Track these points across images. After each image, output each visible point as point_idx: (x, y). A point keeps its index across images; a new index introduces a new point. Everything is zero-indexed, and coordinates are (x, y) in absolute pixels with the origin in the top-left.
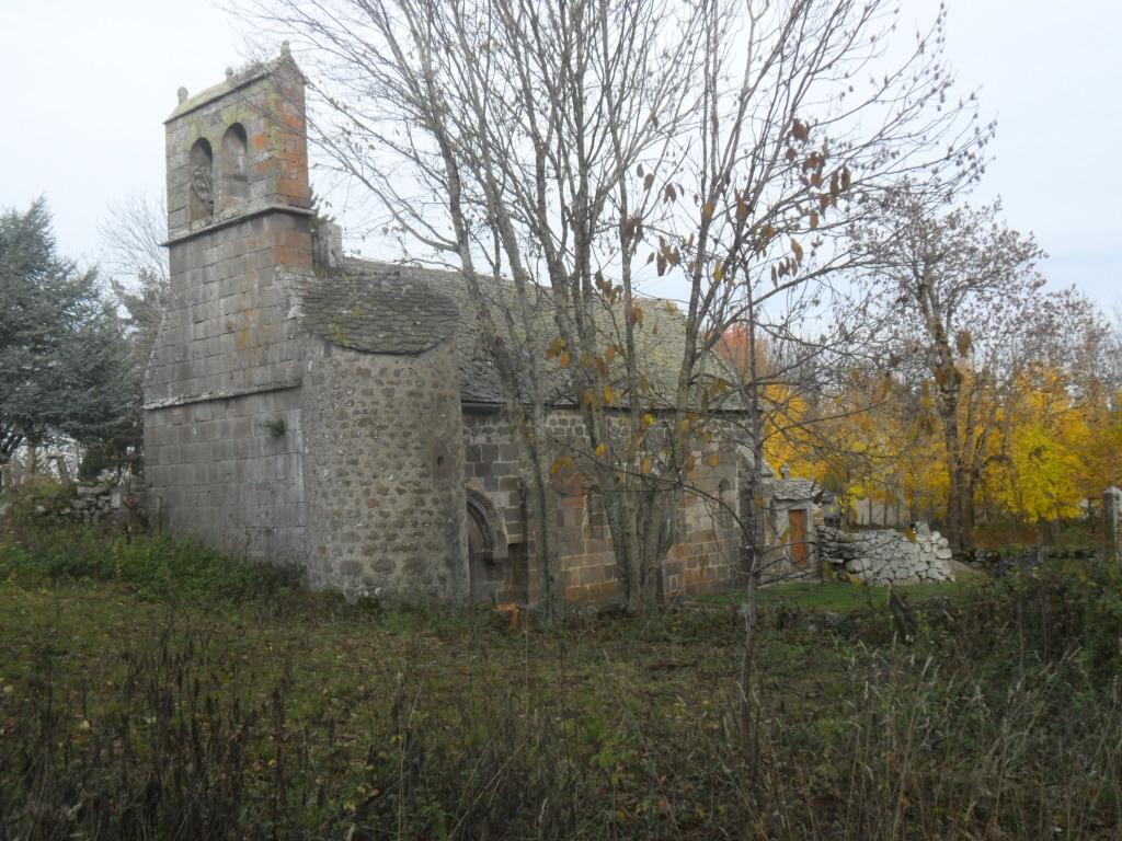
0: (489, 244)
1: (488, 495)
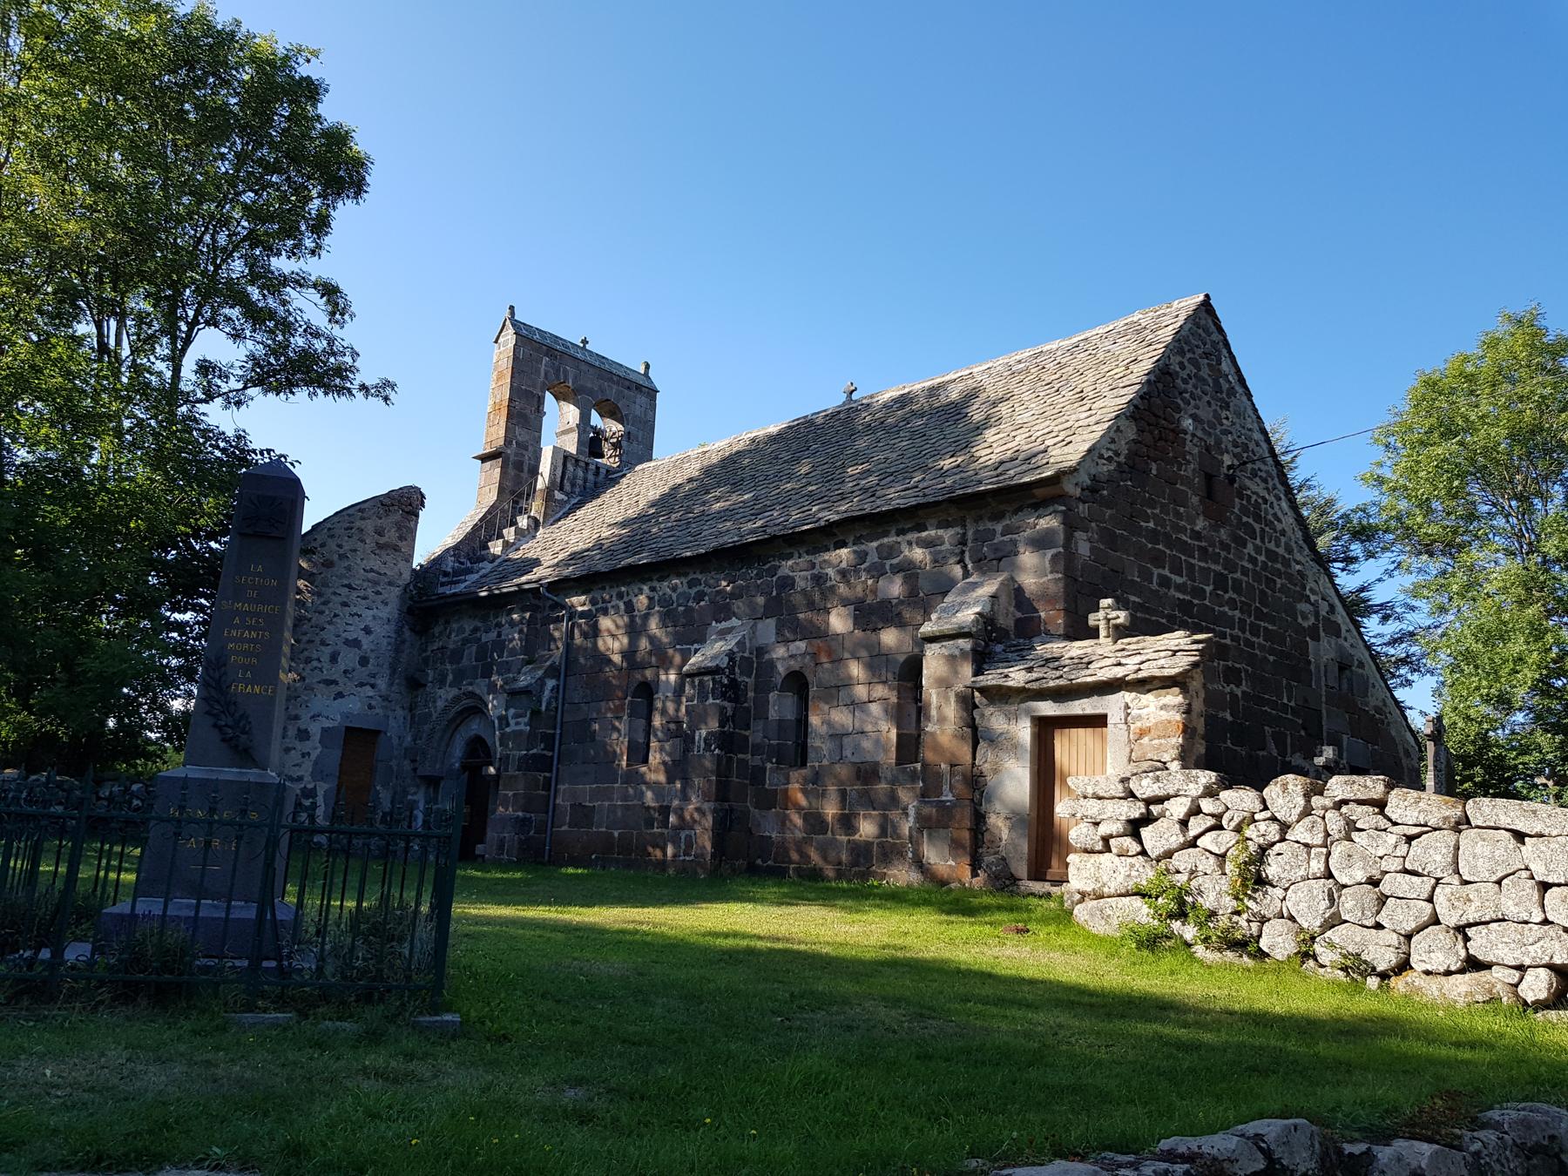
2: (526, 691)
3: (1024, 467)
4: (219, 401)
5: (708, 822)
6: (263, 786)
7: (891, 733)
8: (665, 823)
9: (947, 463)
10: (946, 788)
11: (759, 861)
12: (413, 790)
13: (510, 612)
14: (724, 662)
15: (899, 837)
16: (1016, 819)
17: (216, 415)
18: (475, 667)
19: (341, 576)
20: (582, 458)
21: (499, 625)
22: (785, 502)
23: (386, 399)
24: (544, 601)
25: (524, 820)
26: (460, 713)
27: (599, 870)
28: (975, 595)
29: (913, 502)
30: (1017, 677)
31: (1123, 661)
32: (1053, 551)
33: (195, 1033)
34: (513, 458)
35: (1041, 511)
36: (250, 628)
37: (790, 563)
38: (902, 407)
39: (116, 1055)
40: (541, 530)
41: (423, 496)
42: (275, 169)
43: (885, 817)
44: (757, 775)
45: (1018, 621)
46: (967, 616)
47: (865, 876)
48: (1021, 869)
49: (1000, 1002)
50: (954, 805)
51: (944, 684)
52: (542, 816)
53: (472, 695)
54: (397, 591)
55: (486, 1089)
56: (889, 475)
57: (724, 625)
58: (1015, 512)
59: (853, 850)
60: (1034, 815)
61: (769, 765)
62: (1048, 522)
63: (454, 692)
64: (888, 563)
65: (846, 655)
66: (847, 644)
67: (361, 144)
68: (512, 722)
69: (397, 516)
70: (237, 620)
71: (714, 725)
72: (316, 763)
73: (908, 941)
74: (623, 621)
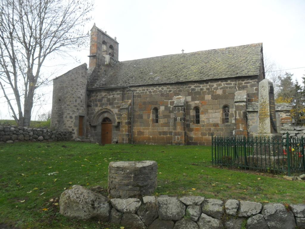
0: (33, 26)
1: (112, 110)
11: (190, 141)
31: (278, 107)
61: (191, 124)
72: (74, 123)
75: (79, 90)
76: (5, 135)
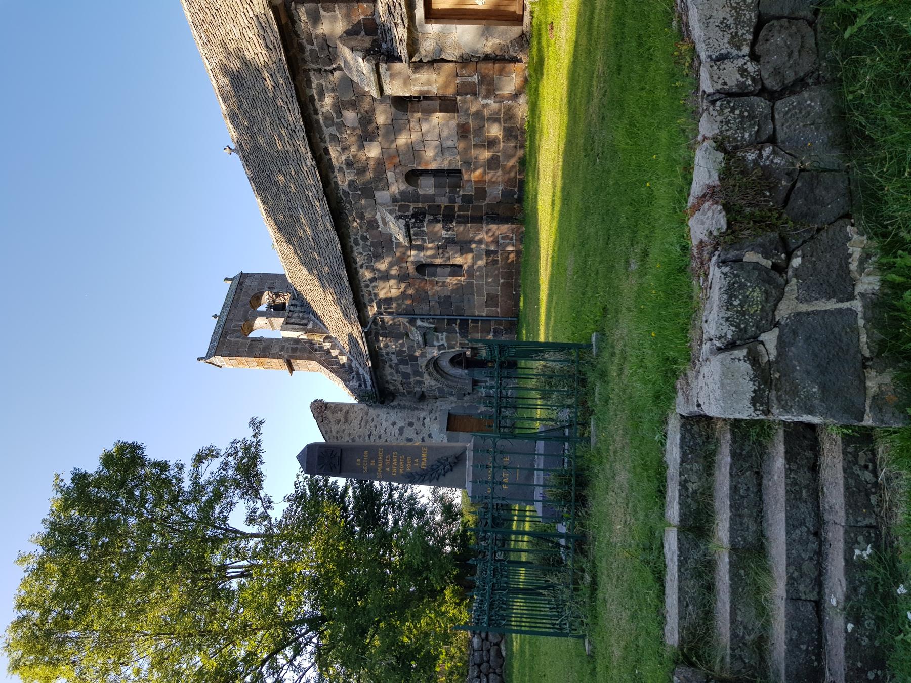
2: (424, 336)
3: (268, 30)
4: (269, 512)
5: (494, 227)
6: (475, 449)
7: (438, 118)
8: (495, 252)
9: (269, 83)
10: (470, 79)
11: (516, 196)
12: (480, 394)
13: (379, 347)
14: (402, 222)
15: (500, 110)
16: (486, 34)
17: (277, 513)
18: (412, 365)
19: (364, 440)
20: (286, 314)
21: (387, 354)
22: (303, 188)
23: (261, 423)
24: (372, 331)
25: (495, 332)
26: (438, 372)
27: (521, 289)
28: (352, 62)
29: (296, 104)
30: (401, 33)
32: (321, 10)
33: (601, 463)
34: (290, 354)
35: (296, 18)
36: (391, 462)
37: (340, 183)
38: (237, 115)
39: (610, 498)
40: (332, 335)
41: (316, 401)
42: (130, 493)
43: (488, 119)
44: (467, 199)
45: (367, 34)
46: (365, 67)
47: (523, 132)
48: (515, 31)
49: (590, 31)
50: (481, 74)
51: (407, 81)
52: (492, 323)
53: (427, 366)
54: (371, 410)
55: (629, 309)
56: (281, 121)
57: (380, 223)
58: (298, 36)
59: (508, 139)
60: (484, 22)
61: (461, 193)
62: (302, 14)
63: (426, 376)
64: (336, 120)
65: (394, 146)
66: (386, 146)
67: (111, 447)
68: (441, 343)
69: (328, 413)
70: (388, 469)
71: (439, 226)
73: (558, 97)
74: (381, 284)
75: (383, 431)
76: (488, 662)
